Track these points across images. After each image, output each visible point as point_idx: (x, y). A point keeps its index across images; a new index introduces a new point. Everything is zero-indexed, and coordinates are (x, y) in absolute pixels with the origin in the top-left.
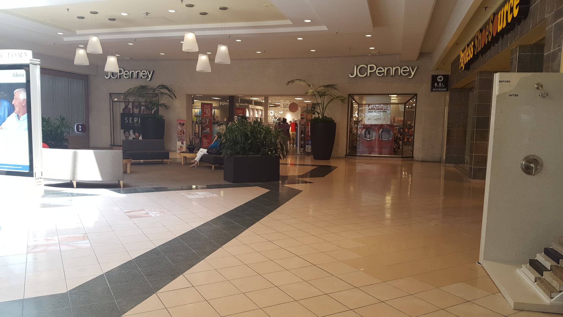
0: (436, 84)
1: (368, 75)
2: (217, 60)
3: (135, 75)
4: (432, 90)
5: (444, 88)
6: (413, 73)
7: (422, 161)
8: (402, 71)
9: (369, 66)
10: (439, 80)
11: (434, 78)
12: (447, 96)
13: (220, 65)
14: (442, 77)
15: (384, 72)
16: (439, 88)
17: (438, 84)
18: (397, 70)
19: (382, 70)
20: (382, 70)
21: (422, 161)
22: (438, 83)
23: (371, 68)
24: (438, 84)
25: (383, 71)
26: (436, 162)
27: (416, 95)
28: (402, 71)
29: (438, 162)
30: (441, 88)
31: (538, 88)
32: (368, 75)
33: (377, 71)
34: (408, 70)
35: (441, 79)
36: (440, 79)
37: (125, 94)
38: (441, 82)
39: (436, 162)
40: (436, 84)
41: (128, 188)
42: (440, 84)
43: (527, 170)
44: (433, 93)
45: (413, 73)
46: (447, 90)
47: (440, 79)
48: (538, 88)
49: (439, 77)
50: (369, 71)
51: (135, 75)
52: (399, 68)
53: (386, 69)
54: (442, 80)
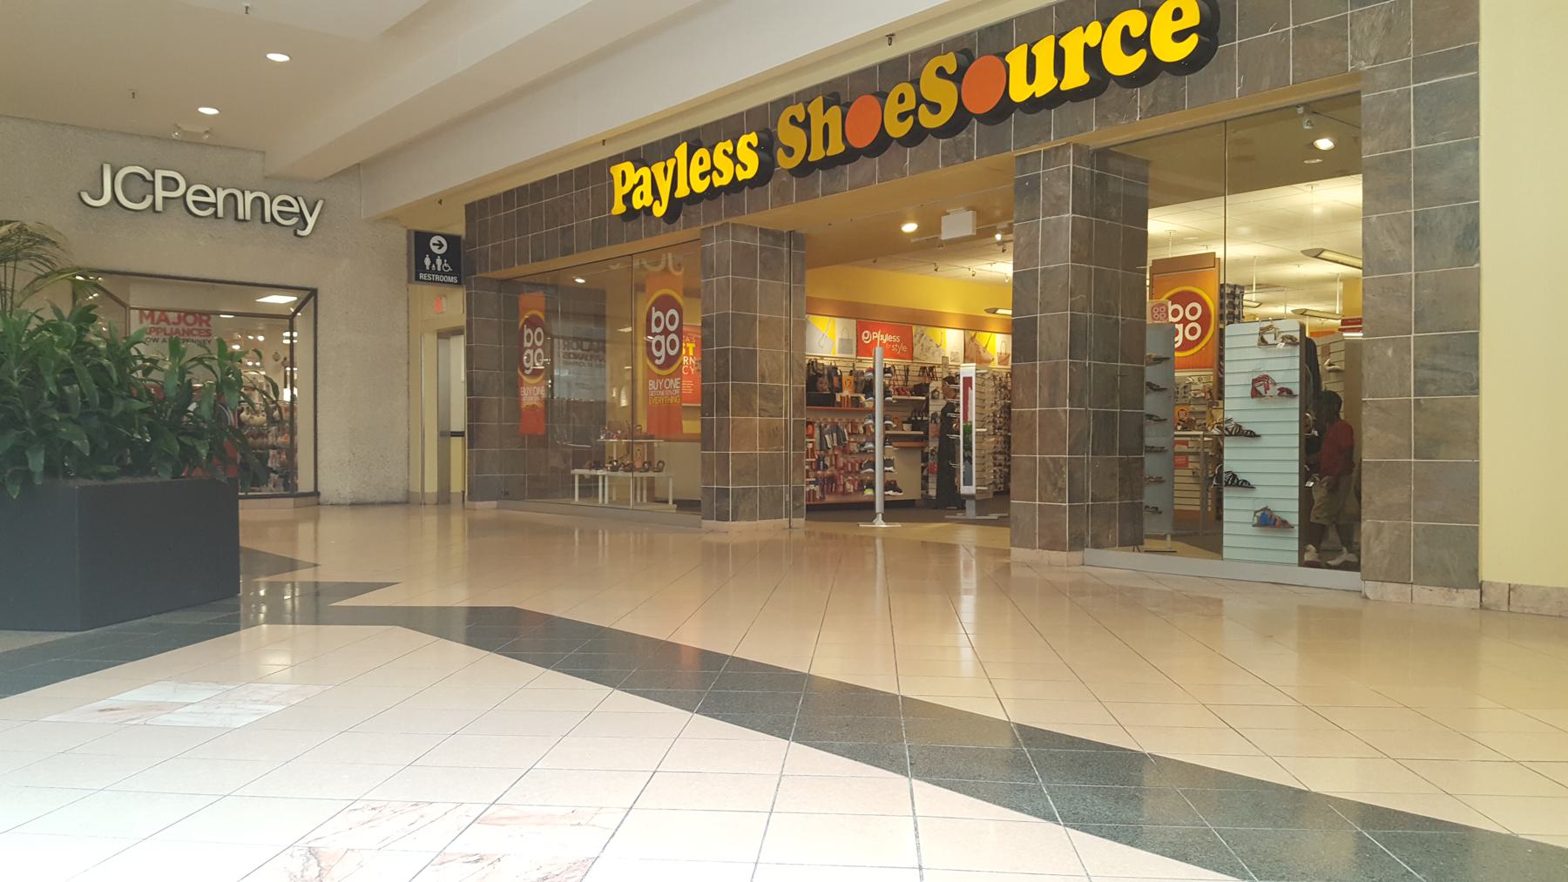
0: (427, 261)
1: (159, 206)
3: (245, 209)
5: (449, 274)
6: (311, 221)
7: (356, 505)
9: (159, 174)
10: (435, 249)
11: (420, 241)
12: (453, 306)
14: (444, 242)
15: (215, 205)
16: (436, 272)
17: (433, 261)
19: (207, 195)
20: (207, 195)
21: (356, 505)
22: (433, 257)
23: (170, 183)
24: (433, 261)
25: (211, 199)
26: (394, 503)
28: (276, 208)
30: (442, 273)
35: (441, 245)
36: (438, 246)
37: (32, 234)
38: (442, 257)
39: (394, 503)
40: (427, 261)
42: (439, 261)
44: (419, 287)
46: (459, 283)
47: (438, 246)
49: (434, 240)
50: (160, 193)
51: (245, 209)
53: (222, 194)
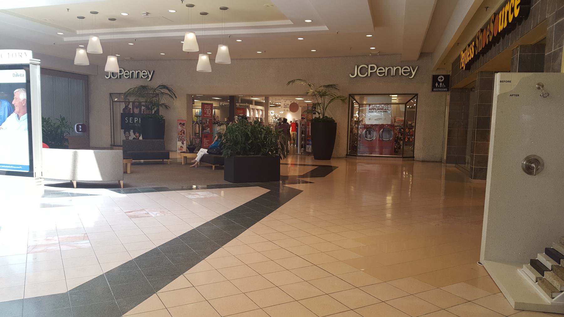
0: (437, 84)
1: (369, 75)
2: (217, 60)
3: (135, 75)
4: (433, 90)
5: (444, 88)
6: (414, 73)
7: (423, 161)
8: (403, 71)
9: (370, 66)
10: (439, 80)
11: (435, 78)
12: (447, 96)
13: (221, 65)
14: (443, 77)
15: (385, 72)
16: (440, 88)
17: (439, 84)
18: (397, 70)
19: (382, 70)
20: (382, 70)
21: (423, 161)
22: (439, 83)
23: (372, 68)
24: (439, 84)
25: (384, 71)
26: (437, 162)
27: (417, 95)
28: (403, 71)
29: (439, 162)
30: (442, 88)
31: (539, 88)
32: (369, 75)
33: (378, 71)
34: (409, 70)
35: (442, 79)
36: (441, 79)
37: (125, 94)
38: (442, 82)
39: (437, 162)
40: (437, 84)
41: (128, 188)
42: (441, 84)
43: (528, 170)
44: (433, 93)
45: (414, 73)
46: (448, 90)
47: (441, 79)
48: (539, 88)
49: (440, 77)
50: (370, 71)
51: (135, 75)
52: (400, 68)
53: (387, 69)
54: (443, 80)
